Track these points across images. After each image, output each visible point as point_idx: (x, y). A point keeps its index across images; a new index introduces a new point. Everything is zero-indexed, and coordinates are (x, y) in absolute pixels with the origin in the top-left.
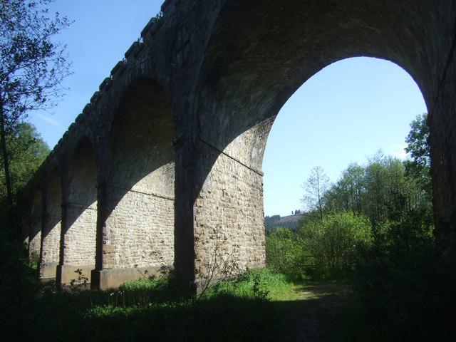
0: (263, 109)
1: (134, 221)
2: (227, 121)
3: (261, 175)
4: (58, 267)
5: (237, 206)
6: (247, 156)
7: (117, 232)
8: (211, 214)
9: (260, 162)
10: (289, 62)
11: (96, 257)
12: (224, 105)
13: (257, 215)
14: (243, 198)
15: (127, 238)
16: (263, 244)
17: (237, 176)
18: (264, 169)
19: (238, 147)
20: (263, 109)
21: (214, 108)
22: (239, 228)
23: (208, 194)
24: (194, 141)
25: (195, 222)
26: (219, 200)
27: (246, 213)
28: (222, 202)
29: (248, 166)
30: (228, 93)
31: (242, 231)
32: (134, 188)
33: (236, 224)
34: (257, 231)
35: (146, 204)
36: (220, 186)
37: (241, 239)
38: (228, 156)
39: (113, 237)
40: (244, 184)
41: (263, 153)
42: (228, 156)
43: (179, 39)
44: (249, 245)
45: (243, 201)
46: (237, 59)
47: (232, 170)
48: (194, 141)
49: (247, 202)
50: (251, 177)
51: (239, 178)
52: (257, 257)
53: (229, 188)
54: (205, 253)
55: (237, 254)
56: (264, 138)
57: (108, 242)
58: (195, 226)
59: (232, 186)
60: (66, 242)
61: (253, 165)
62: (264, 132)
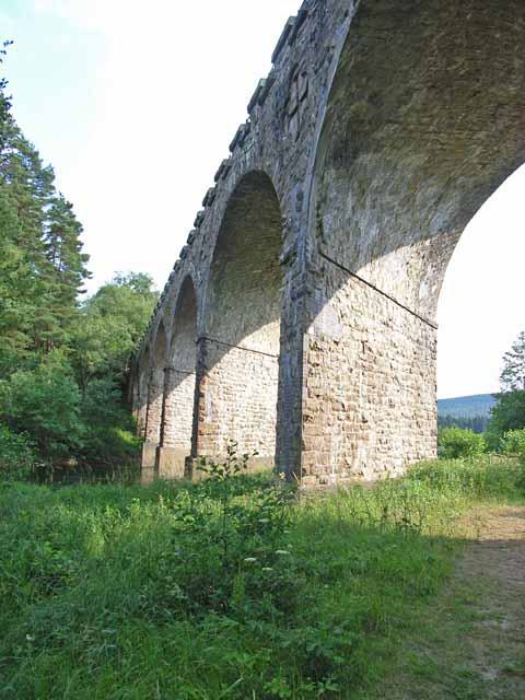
0: (439, 219)
1: (248, 392)
2: (374, 232)
3: (434, 327)
4: (187, 459)
5: (388, 370)
6: (410, 295)
7: (222, 406)
8: (337, 379)
9: (433, 306)
10: (482, 135)
11: (300, 447)
12: (368, 203)
13: (424, 387)
14: (400, 358)
15: (238, 416)
16: (433, 433)
17: (390, 323)
18: (438, 319)
19: (393, 271)
20: (439, 219)
21: (350, 206)
22: (392, 406)
23: (333, 346)
24: (309, 255)
25: (305, 390)
26: (355, 357)
27: (405, 383)
28: (360, 362)
29: (413, 310)
30: (375, 183)
31: (396, 412)
32: (247, 341)
33: (384, 399)
34: (424, 413)
35: (268, 369)
36: (357, 335)
37: (393, 424)
38: (374, 288)
39: (215, 413)
40: (404, 338)
41: (437, 292)
42: (374, 288)
43: (293, 95)
44: (409, 433)
45: (401, 365)
46: (390, 122)
47: (381, 312)
48: (309, 255)
49: (409, 367)
50: (416, 328)
51: (395, 327)
52: (422, 452)
53: (377, 340)
54: (325, 442)
55: (385, 446)
56: (440, 269)
57: (208, 420)
58: (305, 396)
59: (380, 338)
60: (166, 417)
61: (422, 310)
62: (439, 255)
